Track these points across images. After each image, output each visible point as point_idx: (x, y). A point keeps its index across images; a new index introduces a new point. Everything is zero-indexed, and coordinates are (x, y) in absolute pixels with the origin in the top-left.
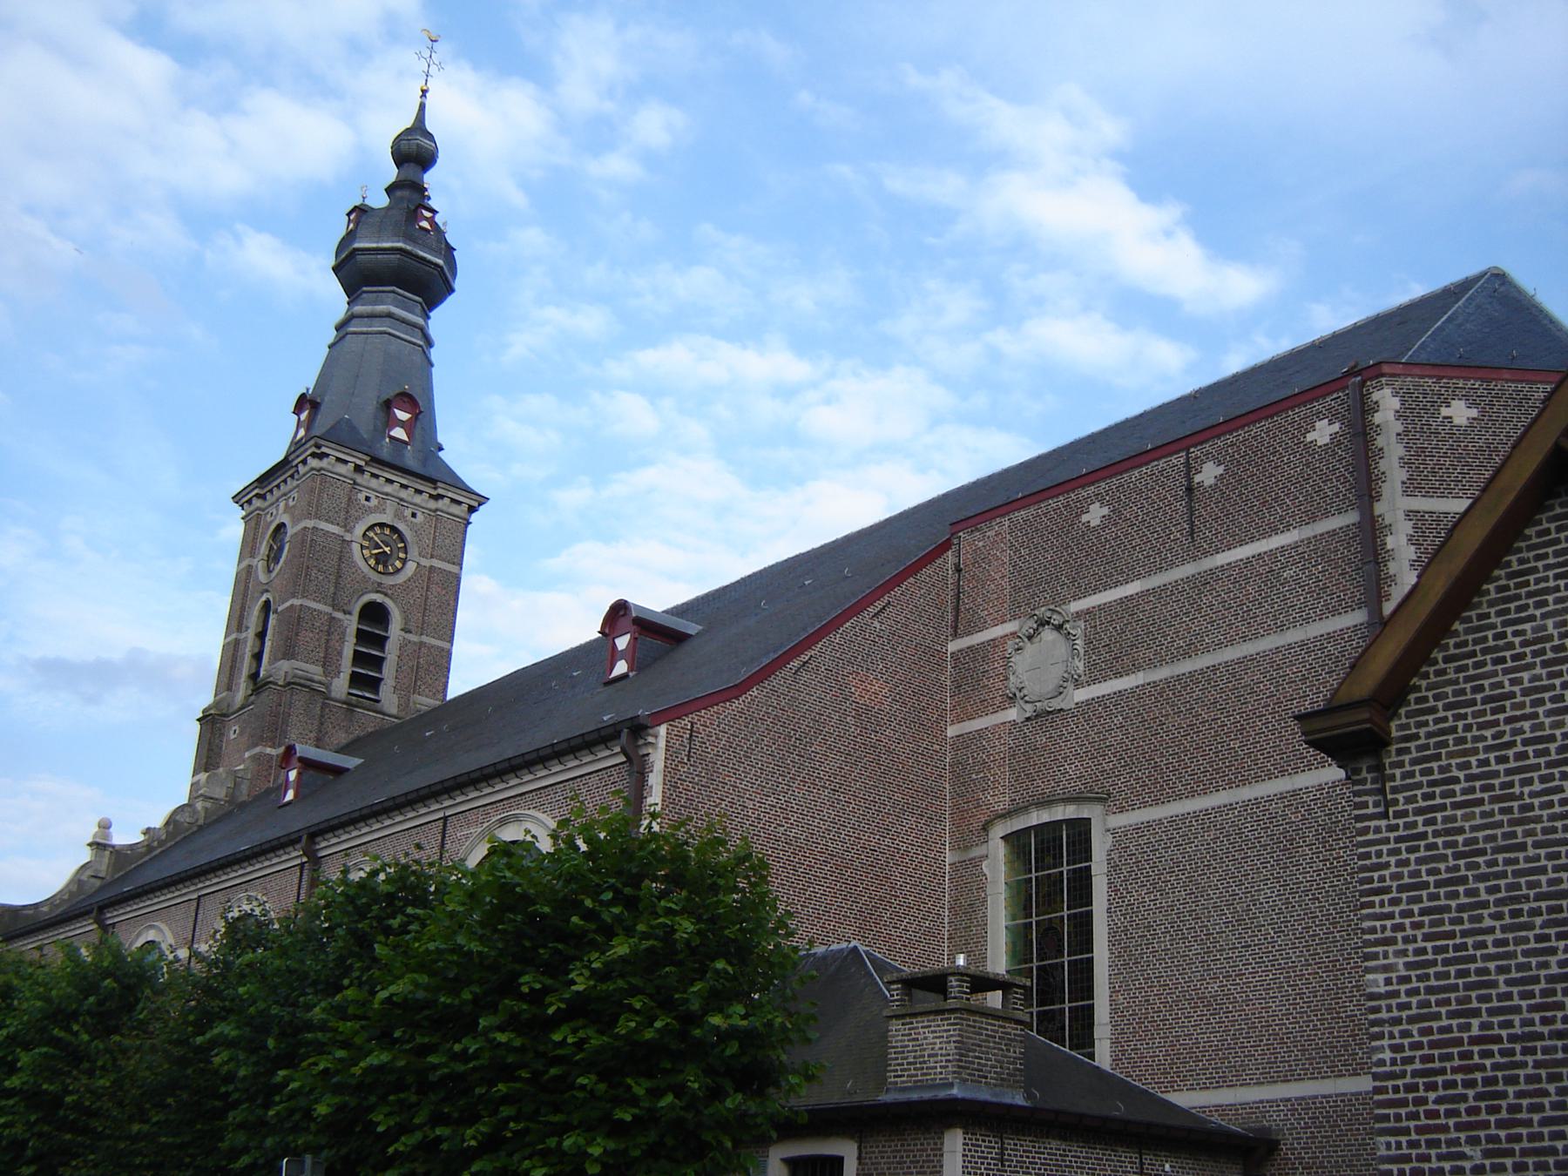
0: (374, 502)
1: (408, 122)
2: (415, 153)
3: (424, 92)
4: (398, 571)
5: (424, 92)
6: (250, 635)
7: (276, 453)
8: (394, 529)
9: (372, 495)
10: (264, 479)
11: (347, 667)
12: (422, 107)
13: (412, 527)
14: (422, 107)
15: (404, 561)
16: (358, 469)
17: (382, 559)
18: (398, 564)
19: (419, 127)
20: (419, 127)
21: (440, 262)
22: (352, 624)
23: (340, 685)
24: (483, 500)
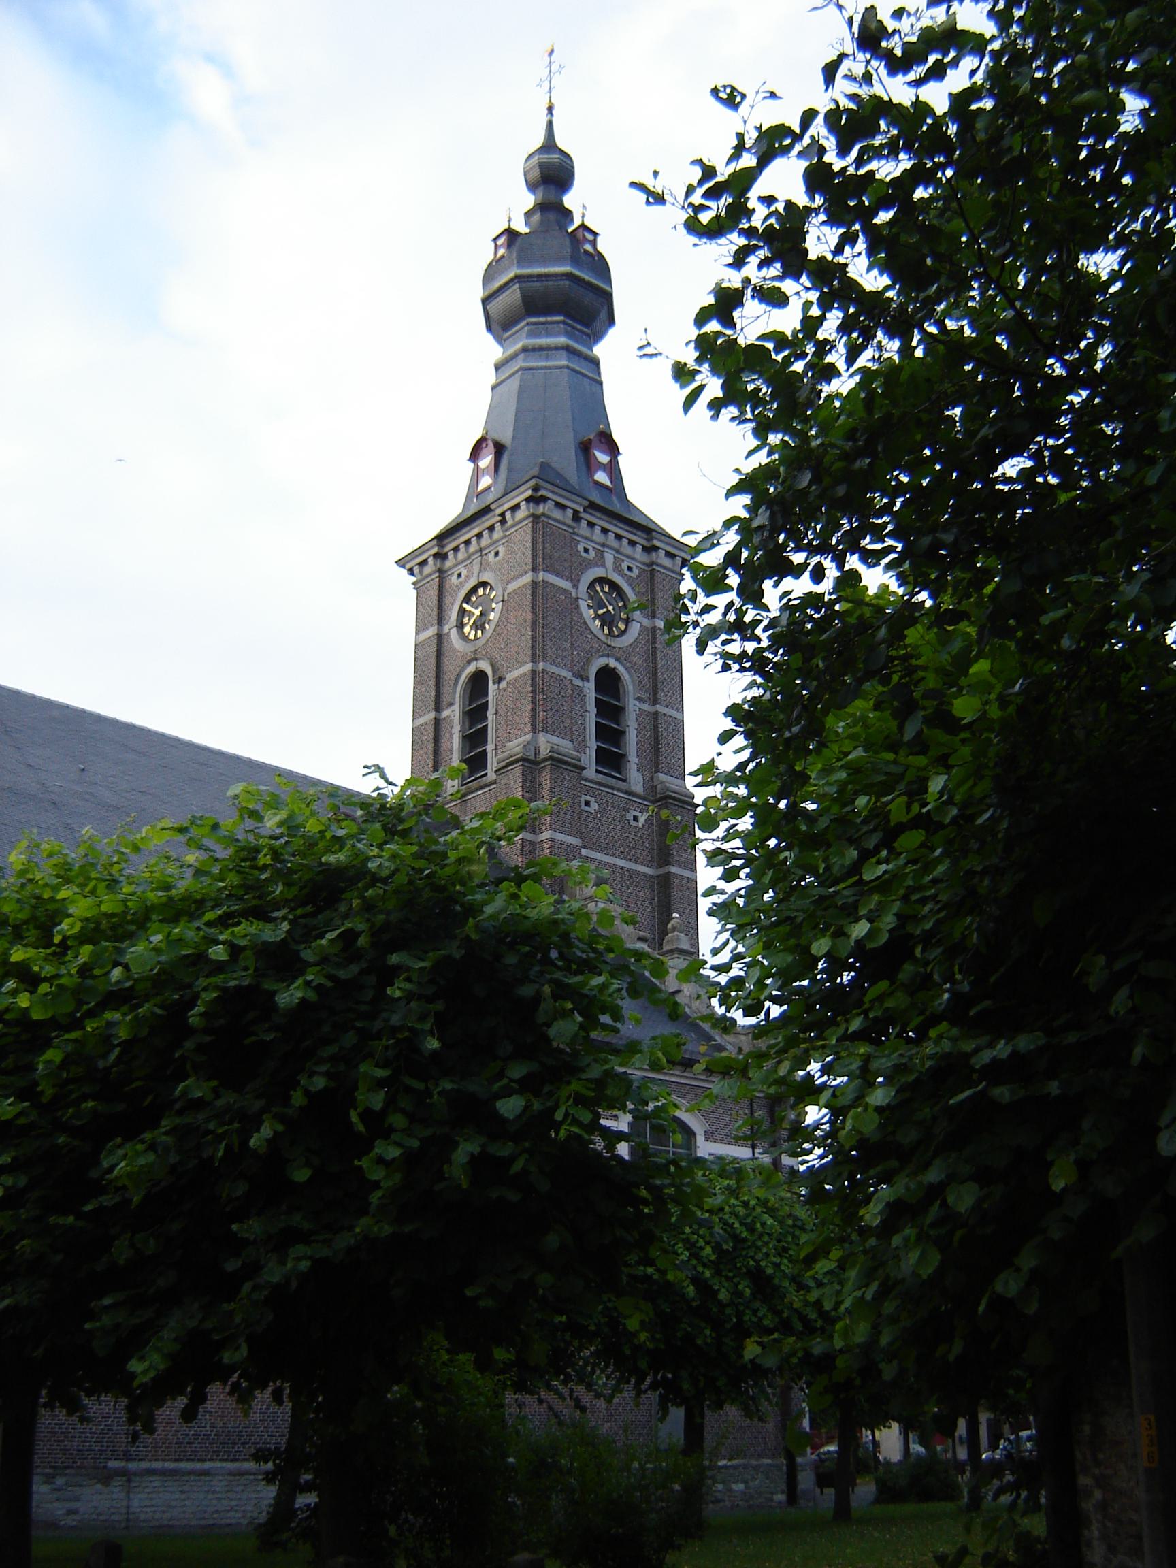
0: (592, 554)
1: (538, 140)
2: (552, 174)
3: (550, 109)
4: (623, 633)
5: (550, 109)
6: (454, 714)
7: (451, 508)
8: (614, 586)
9: (590, 546)
10: (442, 537)
11: (592, 743)
12: (550, 124)
13: (629, 580)
14: (550, 124)
15: (627, 621)
16: (576, 517)
17: (607, 621)
18: (622, 626)
19: (550, 144)
20: (550, 144)
21: (566, 269)
22: (590, 688)
23: (589, 759)
24: (401, 563)
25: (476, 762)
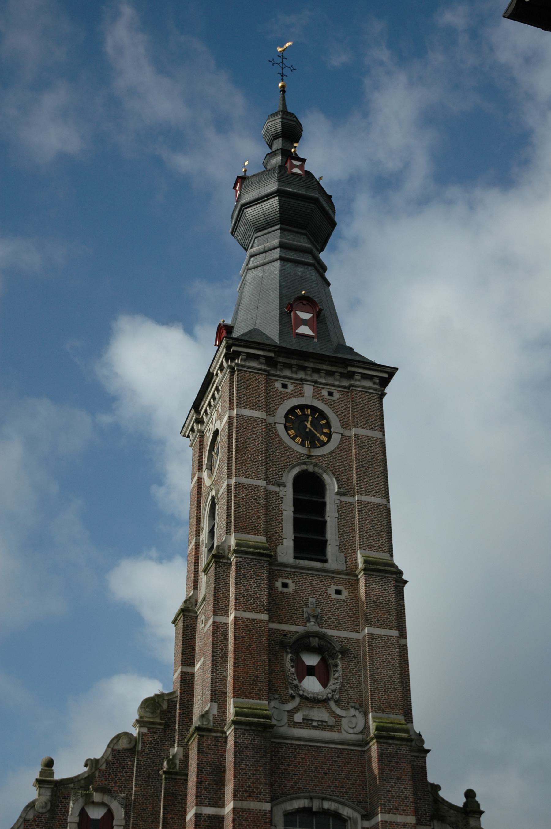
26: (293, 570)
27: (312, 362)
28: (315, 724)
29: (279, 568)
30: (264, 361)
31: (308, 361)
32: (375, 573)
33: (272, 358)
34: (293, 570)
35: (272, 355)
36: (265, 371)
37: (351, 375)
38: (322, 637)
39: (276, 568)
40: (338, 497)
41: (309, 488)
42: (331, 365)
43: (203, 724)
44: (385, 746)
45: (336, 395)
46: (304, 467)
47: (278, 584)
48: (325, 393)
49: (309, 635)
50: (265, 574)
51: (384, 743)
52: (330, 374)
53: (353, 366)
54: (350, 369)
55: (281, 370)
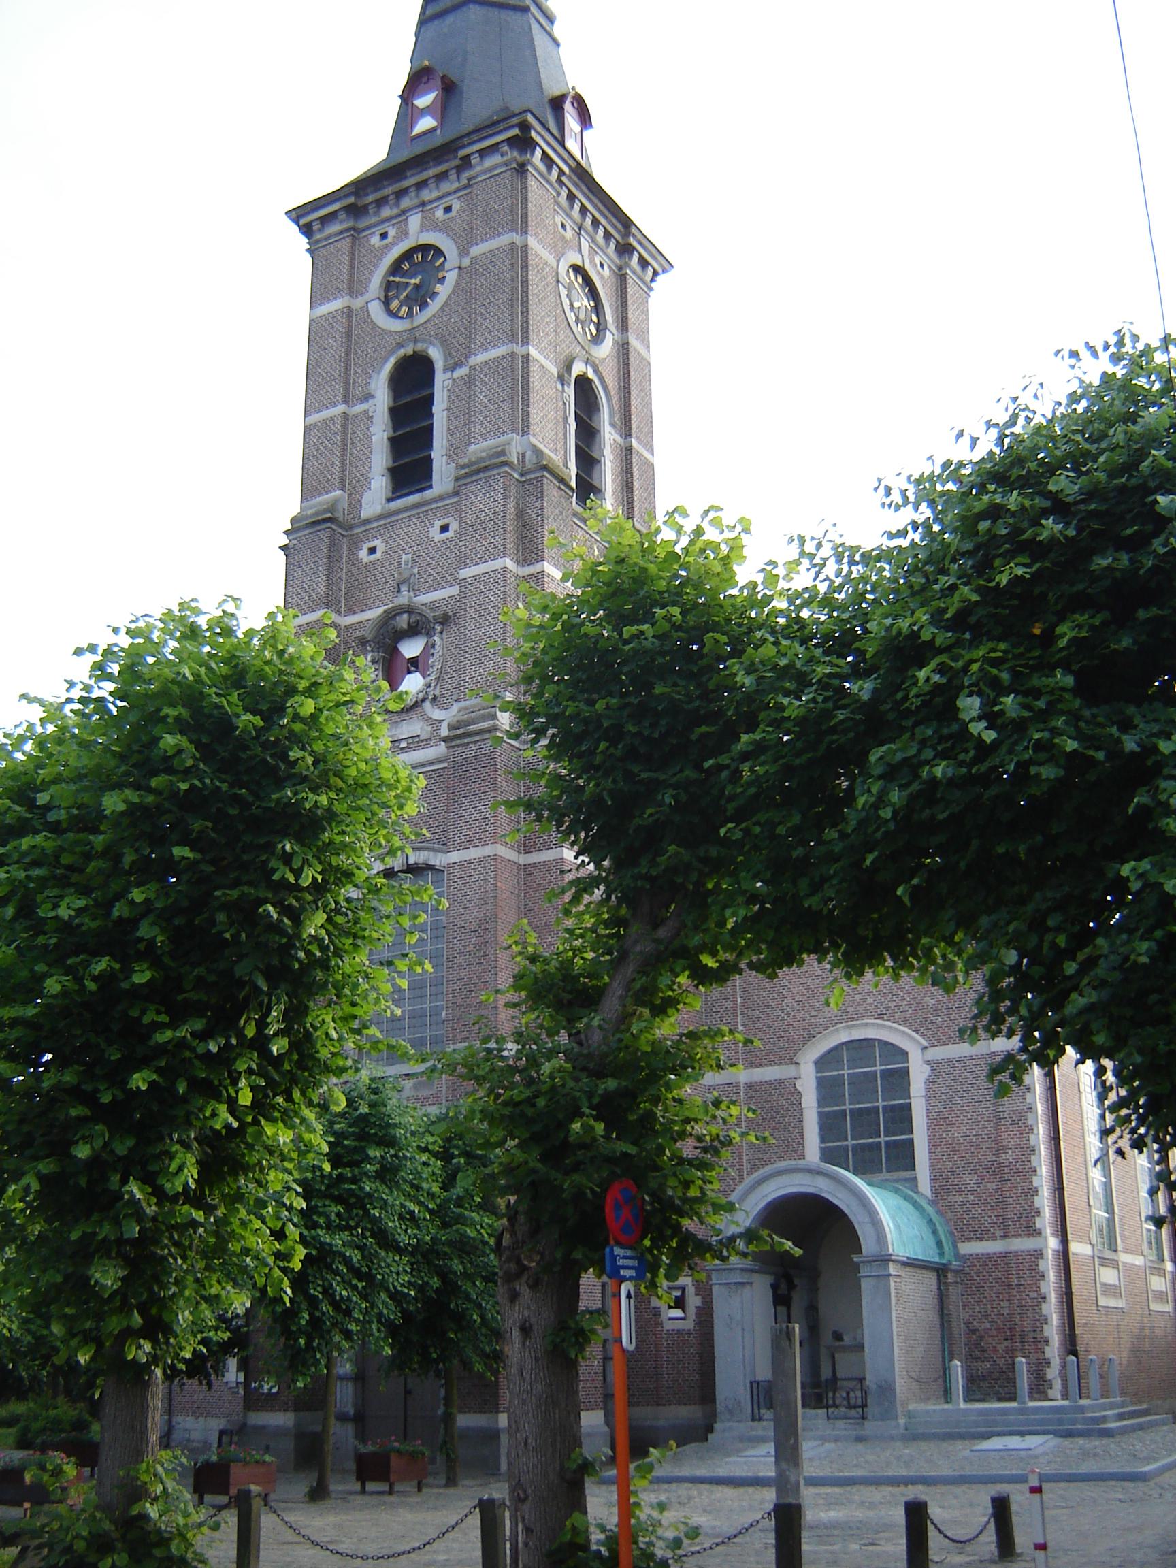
25: (410, 471)
26: (382, 522)
27: (412, 175)
28: (403, 744)
29: (363, 529)
30: (344, 216)
31: (405, 178)
32: (474, 478)
33: (352, 205)
34: (382, 522)
35: (351, 200)
36: (348, 230)
37: (466, 162)
38: (409, 610)
39: (360, 530)
40: (449, 374)
41: (413, 378)
42: (440, 164)
43: (961, 764)
44: (460, 750)
45: (456, 206)
46: (402, 352)
47: (363, 553)
48: (439, 214)
49: (390, 615)
50: (324, 548)
51: (458, 746)
52: (442, 177)
53: (464, 146)
54: (461, 153)
55: (377, 213)
